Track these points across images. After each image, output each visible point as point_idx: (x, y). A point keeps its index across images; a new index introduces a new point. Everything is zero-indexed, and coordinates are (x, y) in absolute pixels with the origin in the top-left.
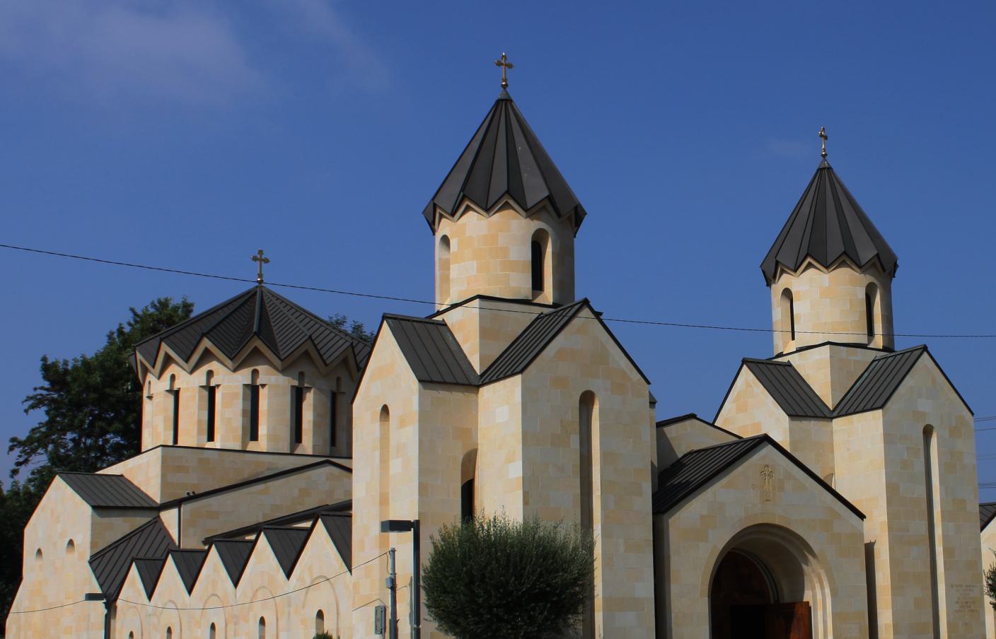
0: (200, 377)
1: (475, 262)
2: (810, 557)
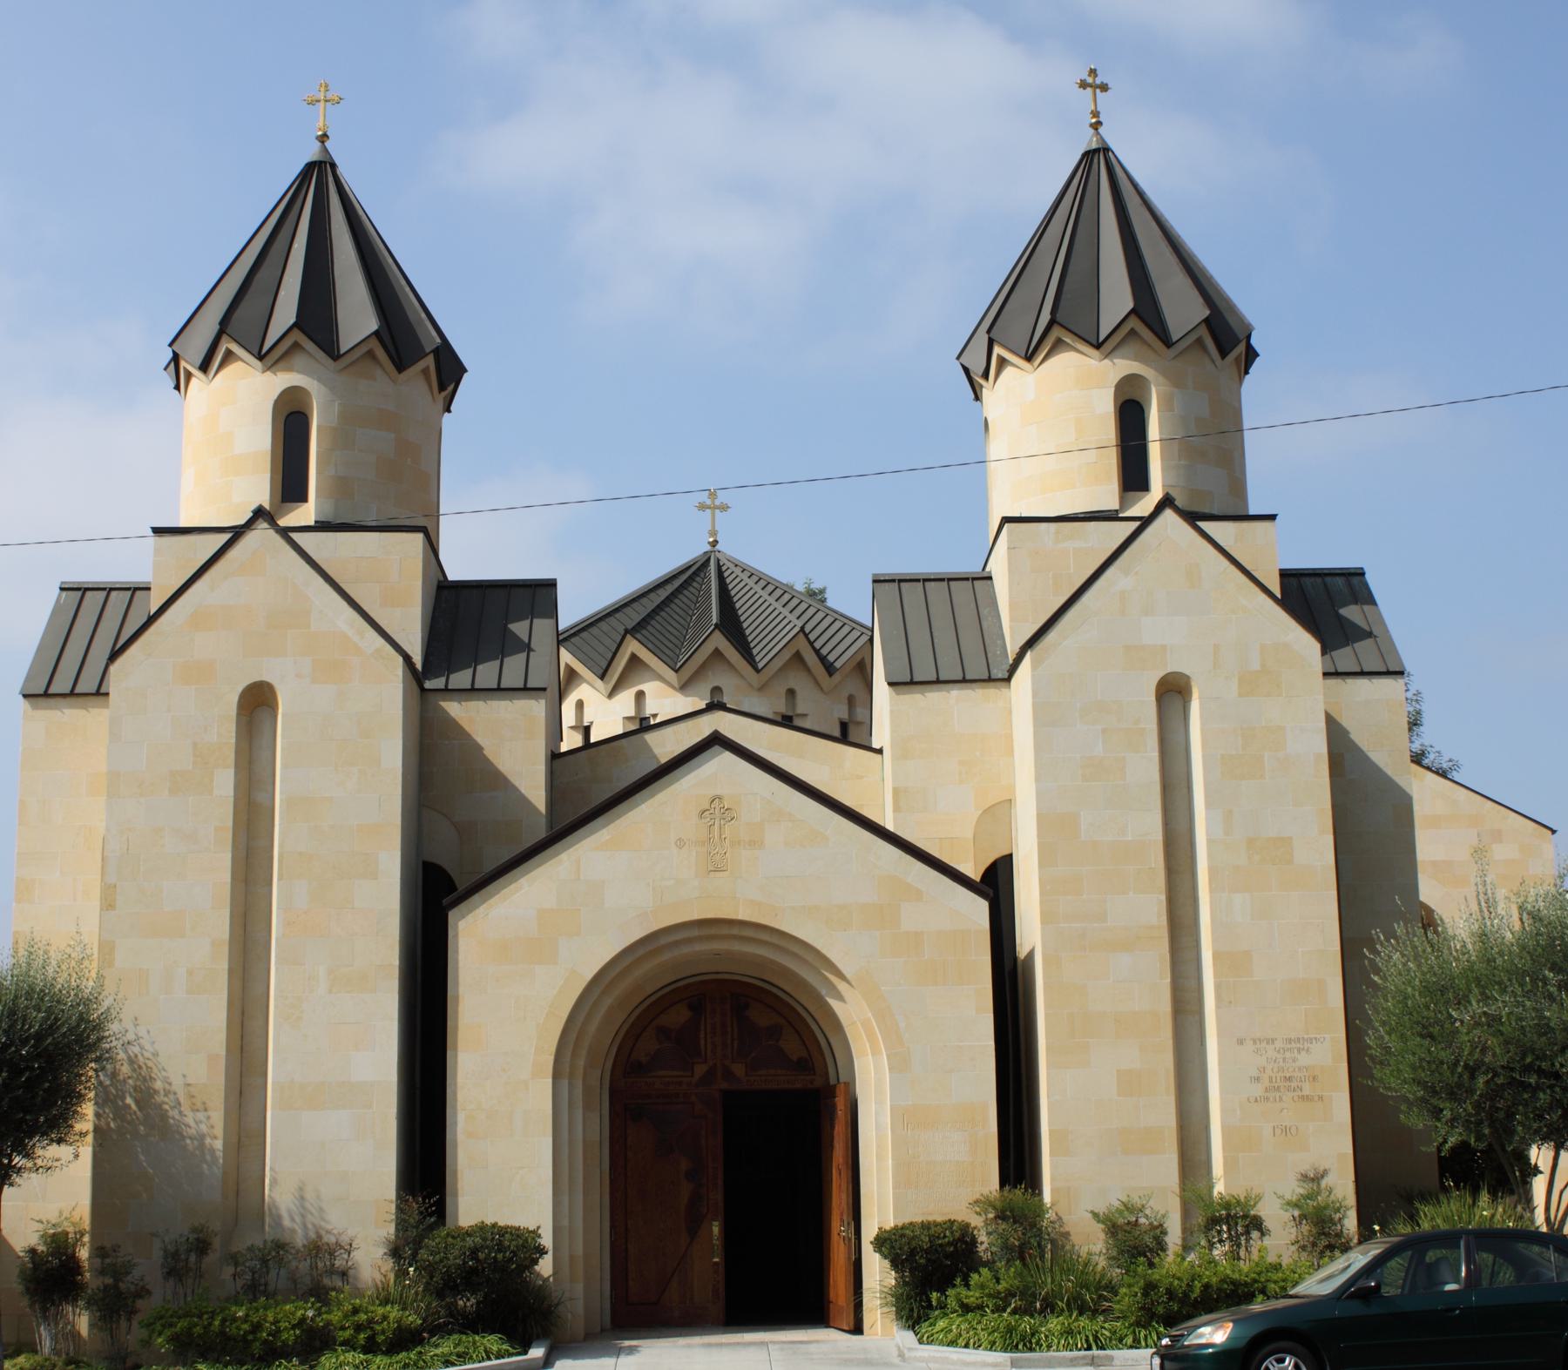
2: (842, 986)
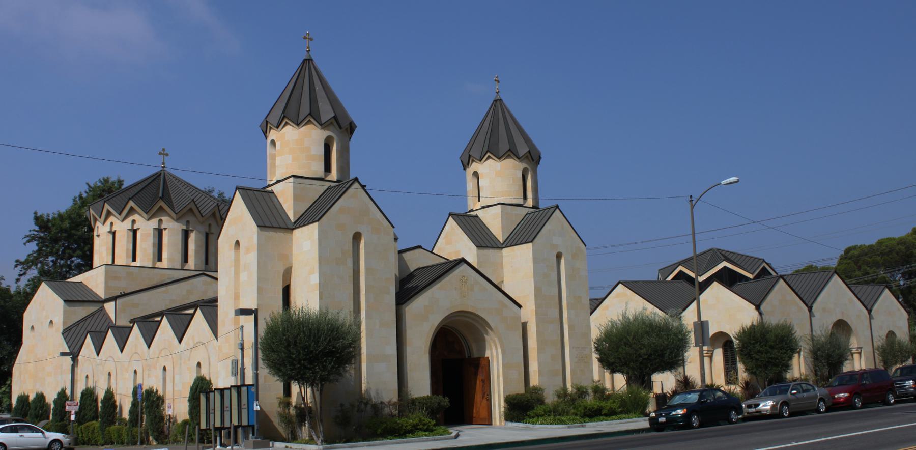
0: (127, 224)
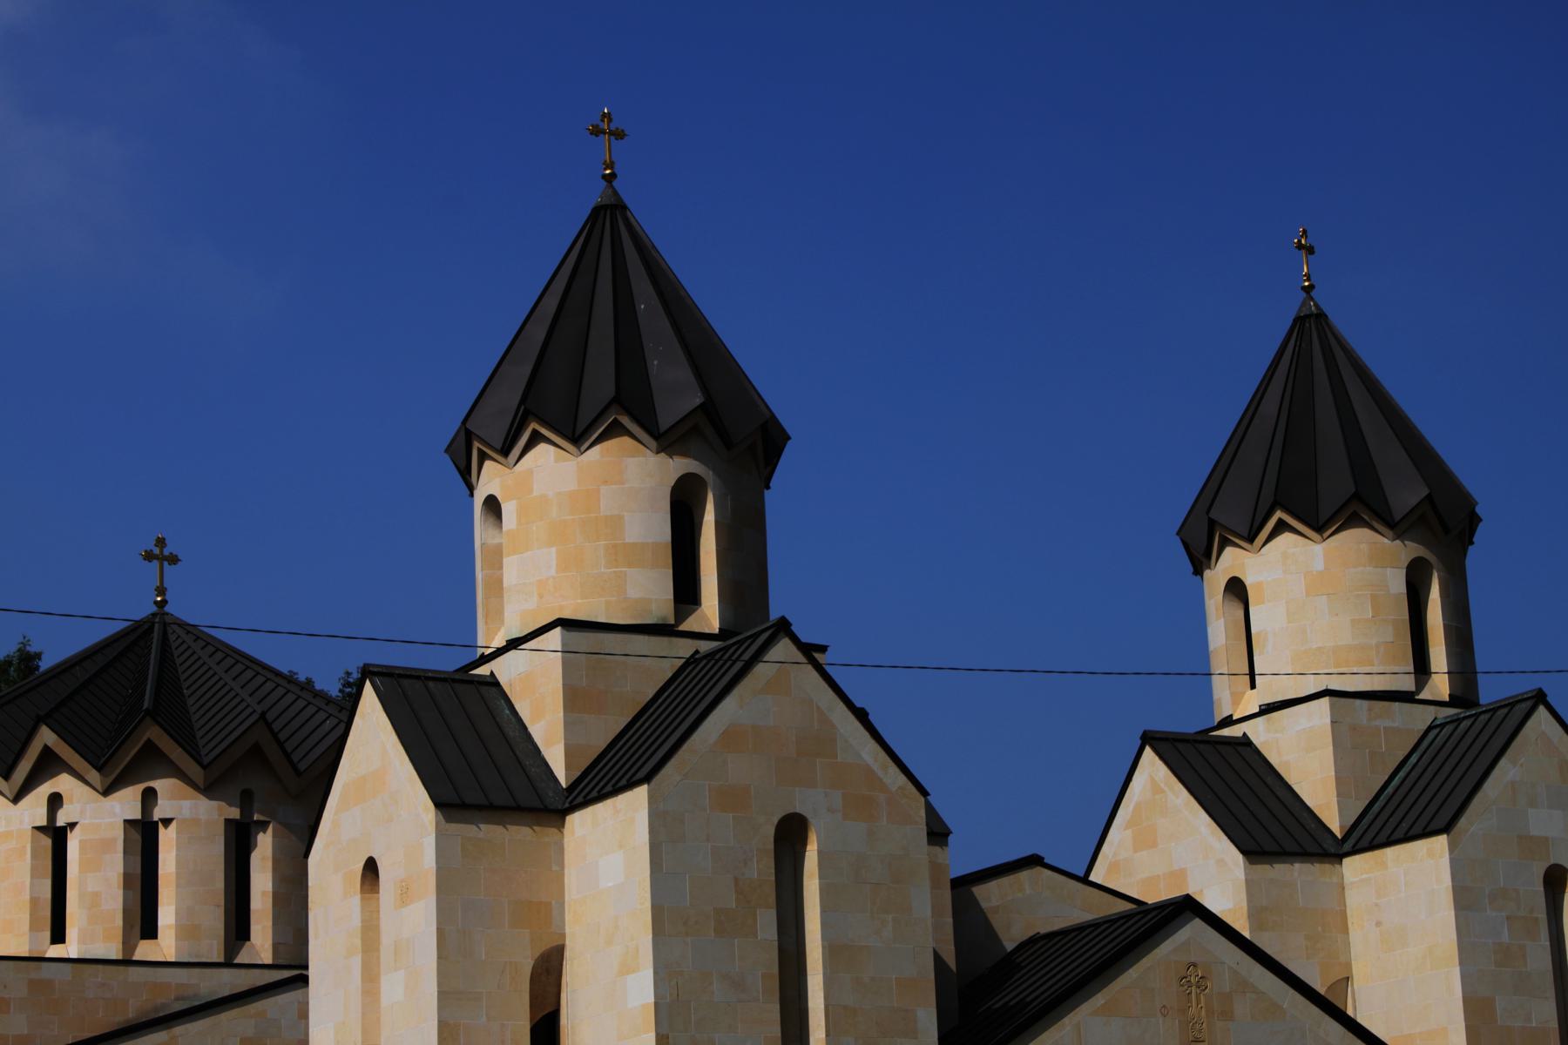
0: (126, 804)
1: (554, 550)
